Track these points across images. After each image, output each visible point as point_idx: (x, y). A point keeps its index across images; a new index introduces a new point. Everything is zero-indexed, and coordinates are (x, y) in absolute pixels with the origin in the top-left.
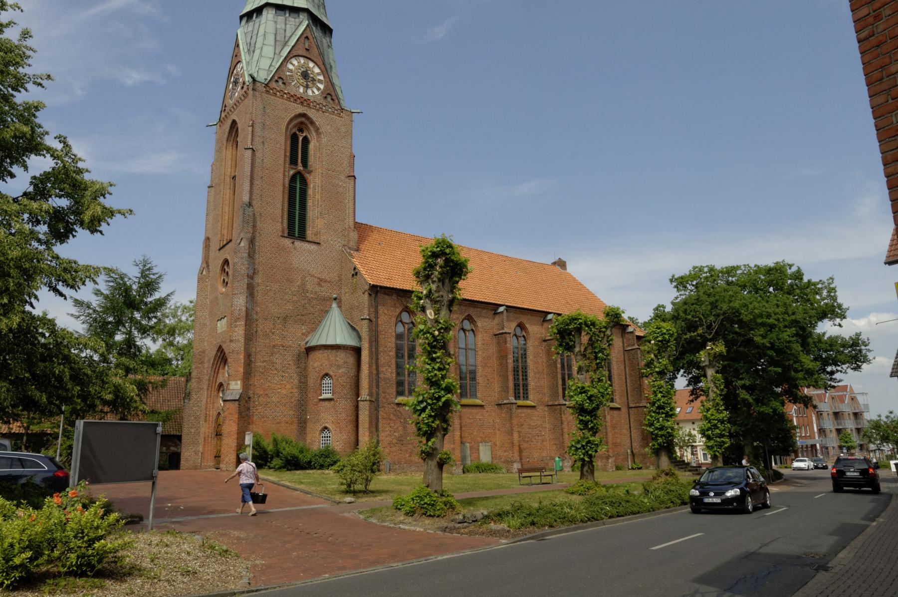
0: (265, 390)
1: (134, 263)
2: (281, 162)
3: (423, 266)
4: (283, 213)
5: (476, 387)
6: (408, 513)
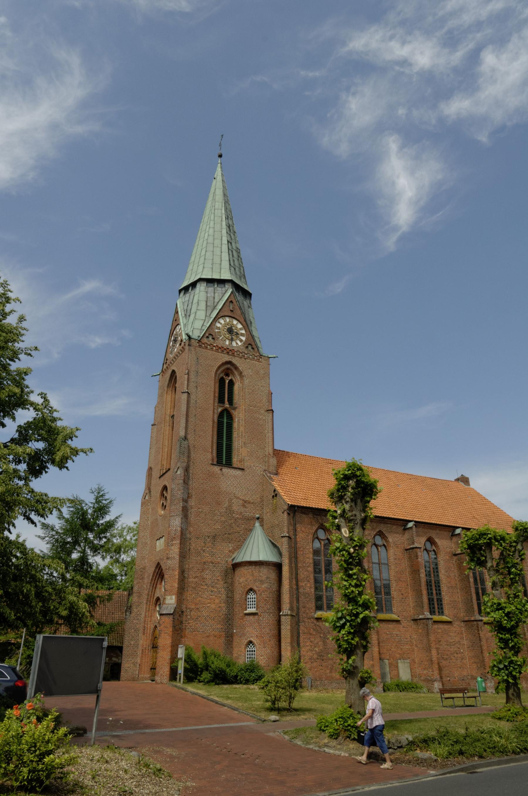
0: (196, 604)
1: (91, 491)
2: (211, 402)
3: (336, 488)
4: (212, 444)
5: (391, 602)
6: (332, 736)
